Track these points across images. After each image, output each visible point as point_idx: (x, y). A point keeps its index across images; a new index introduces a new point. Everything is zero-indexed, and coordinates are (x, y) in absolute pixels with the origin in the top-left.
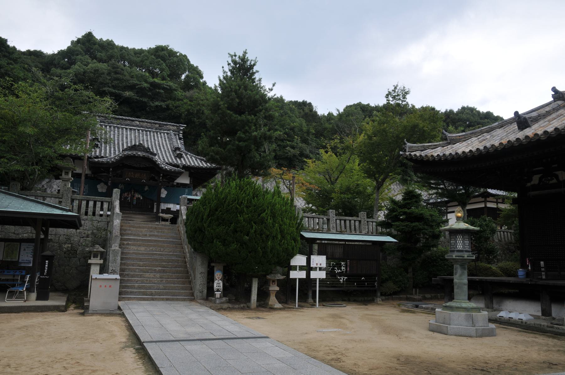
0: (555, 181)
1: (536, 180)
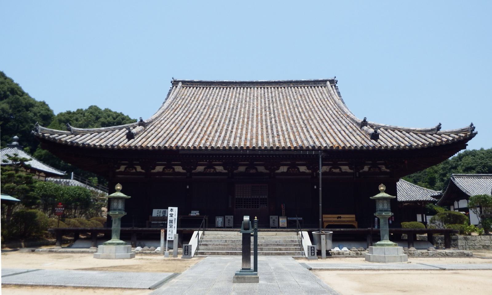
0: (134, 171)
1: (122, 168)
